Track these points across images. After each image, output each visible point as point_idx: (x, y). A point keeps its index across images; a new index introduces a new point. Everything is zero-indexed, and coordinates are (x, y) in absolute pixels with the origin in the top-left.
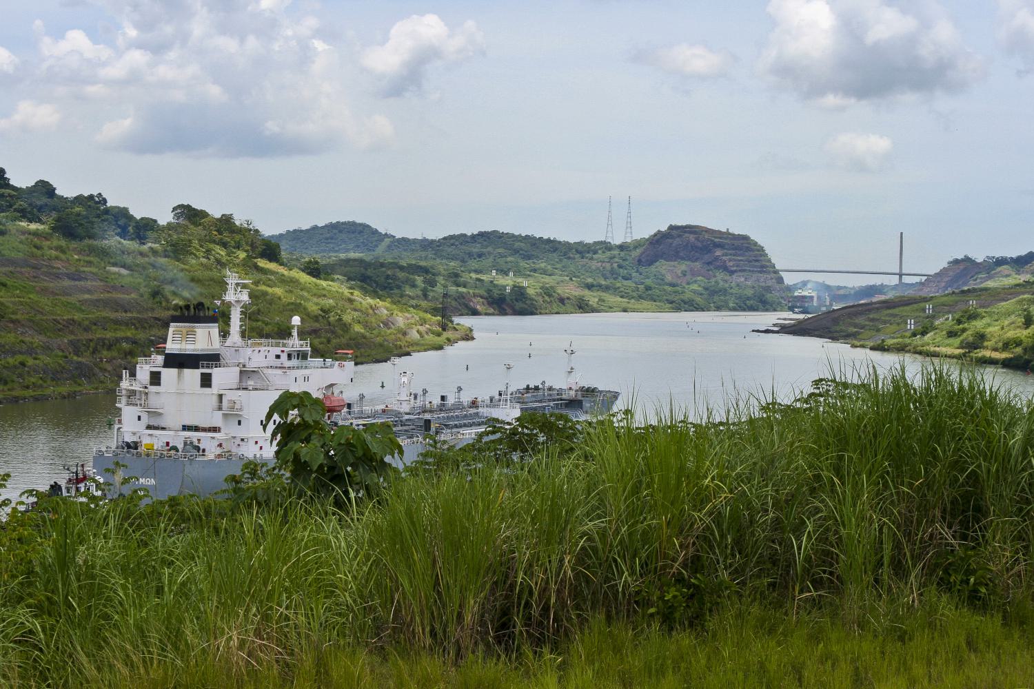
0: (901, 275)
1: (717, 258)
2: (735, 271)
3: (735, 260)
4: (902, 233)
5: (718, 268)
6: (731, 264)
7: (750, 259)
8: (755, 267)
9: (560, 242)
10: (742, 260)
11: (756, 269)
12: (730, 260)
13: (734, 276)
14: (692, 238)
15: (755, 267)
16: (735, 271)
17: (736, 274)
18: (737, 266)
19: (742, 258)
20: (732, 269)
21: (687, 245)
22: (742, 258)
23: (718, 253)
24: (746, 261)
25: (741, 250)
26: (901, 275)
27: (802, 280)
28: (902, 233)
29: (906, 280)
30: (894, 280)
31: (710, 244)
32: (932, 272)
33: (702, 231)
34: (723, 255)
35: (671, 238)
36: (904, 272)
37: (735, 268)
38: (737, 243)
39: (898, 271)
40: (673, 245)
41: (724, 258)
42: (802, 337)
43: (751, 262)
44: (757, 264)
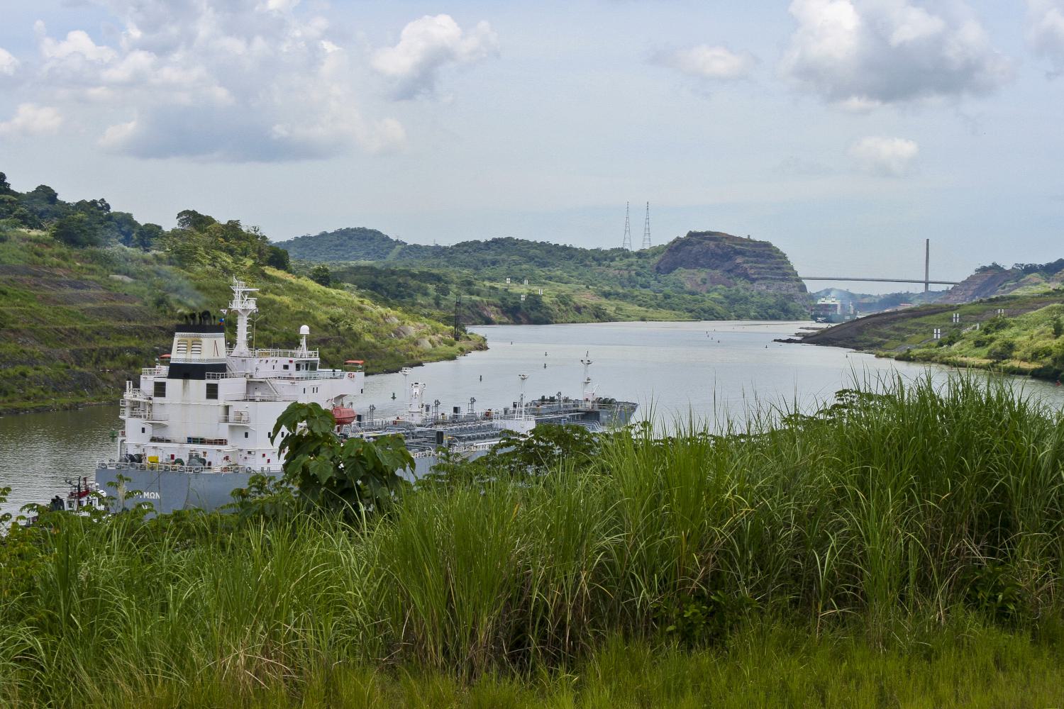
0: (927, 283)
1: (737, 266)
2: (757, 279)
3: (757, 268)
4: (928, 240)
5: (738, 276)
6: (752, 271)
7: (772, 266)
8: (777, 274)
9: (576, 249)
10: (763, 268)
11: (778, 277)
12: (751, 268)
13: (755, 284)
14: (712, 244)
15: (777, 274)
16: (757, 279)
17: (757, 282)
18: (758, 274)
19: (763, 266)
20: (754, 277)
21: (707, 252)
22: (763, 266)
23: (739, 260)
24: (768, 268)
25: (763, 257)
26: (927, 283)
27: (825, 288)
28: (928, 240)
29: (933, 288)
30: (920, 288)
31: (731, 251)
32: (959, 280)
33: (723, 238)
34: (744, 263)
35: (691, 245)
36: (930, 280)
37: (756, 276)
38: (758, 250)
39: (924, 279)
40: (693, 252)
41: (745, 265)
42: (826, 347)
43: (772, 269)
44: (779, 271)
